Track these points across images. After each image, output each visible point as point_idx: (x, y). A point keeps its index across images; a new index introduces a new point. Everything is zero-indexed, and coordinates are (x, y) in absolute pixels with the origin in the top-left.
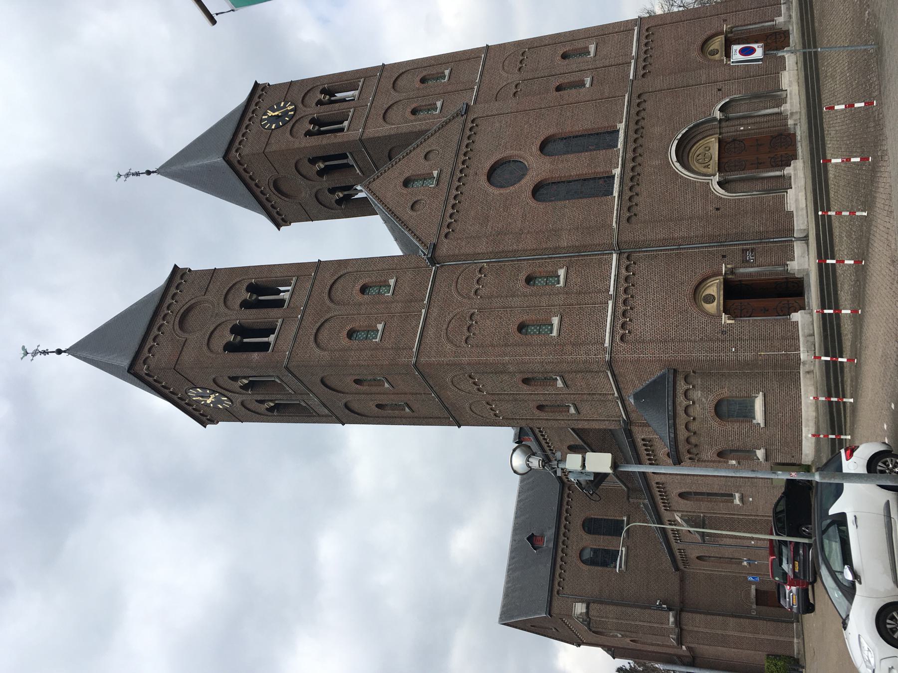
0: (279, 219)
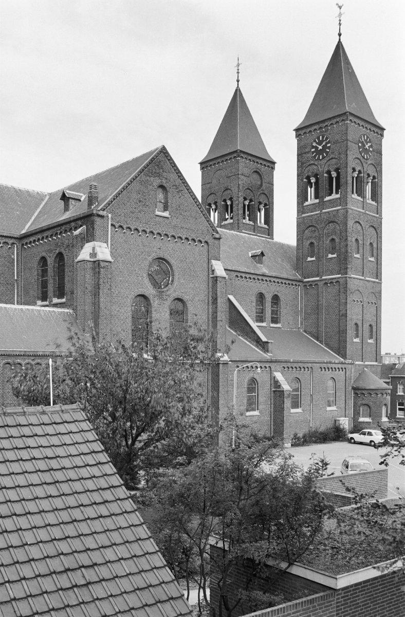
0: (302, 132)
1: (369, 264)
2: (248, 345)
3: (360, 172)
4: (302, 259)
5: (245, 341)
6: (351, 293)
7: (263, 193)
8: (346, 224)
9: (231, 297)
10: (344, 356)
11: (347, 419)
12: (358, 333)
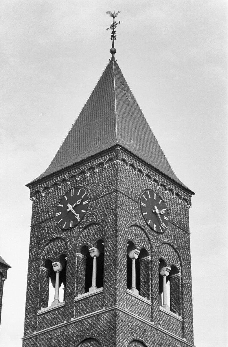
0: (40, 188)
3: (143, 252)
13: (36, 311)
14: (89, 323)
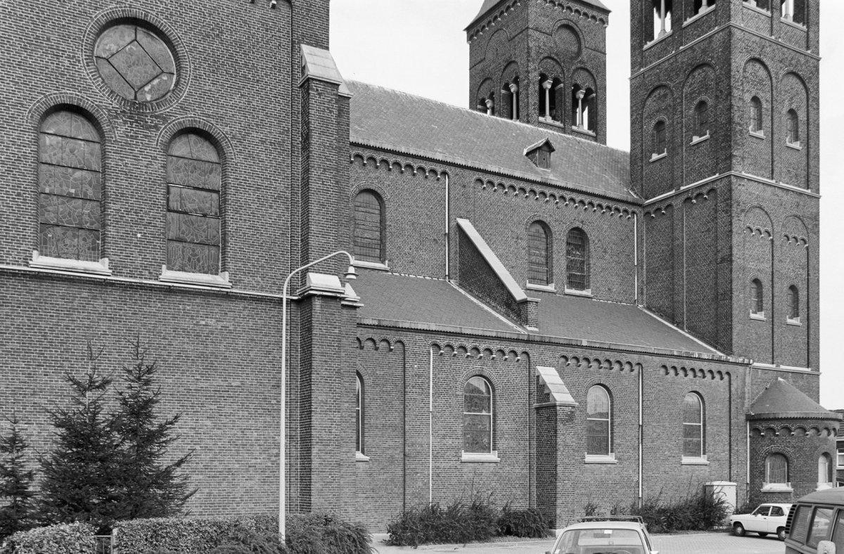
1: (786, 155)
2: (486, 312)
3: (556, 81)
4: (642, 160)
5: (469, 296)
6: (743, 211)
7: (581, 68)
8: (728, 62)
9: (466, 224)
10: (727, 348)
11: (735, 484)
12: (762, 301)
13: (642, 47)
14: (700, 48)
